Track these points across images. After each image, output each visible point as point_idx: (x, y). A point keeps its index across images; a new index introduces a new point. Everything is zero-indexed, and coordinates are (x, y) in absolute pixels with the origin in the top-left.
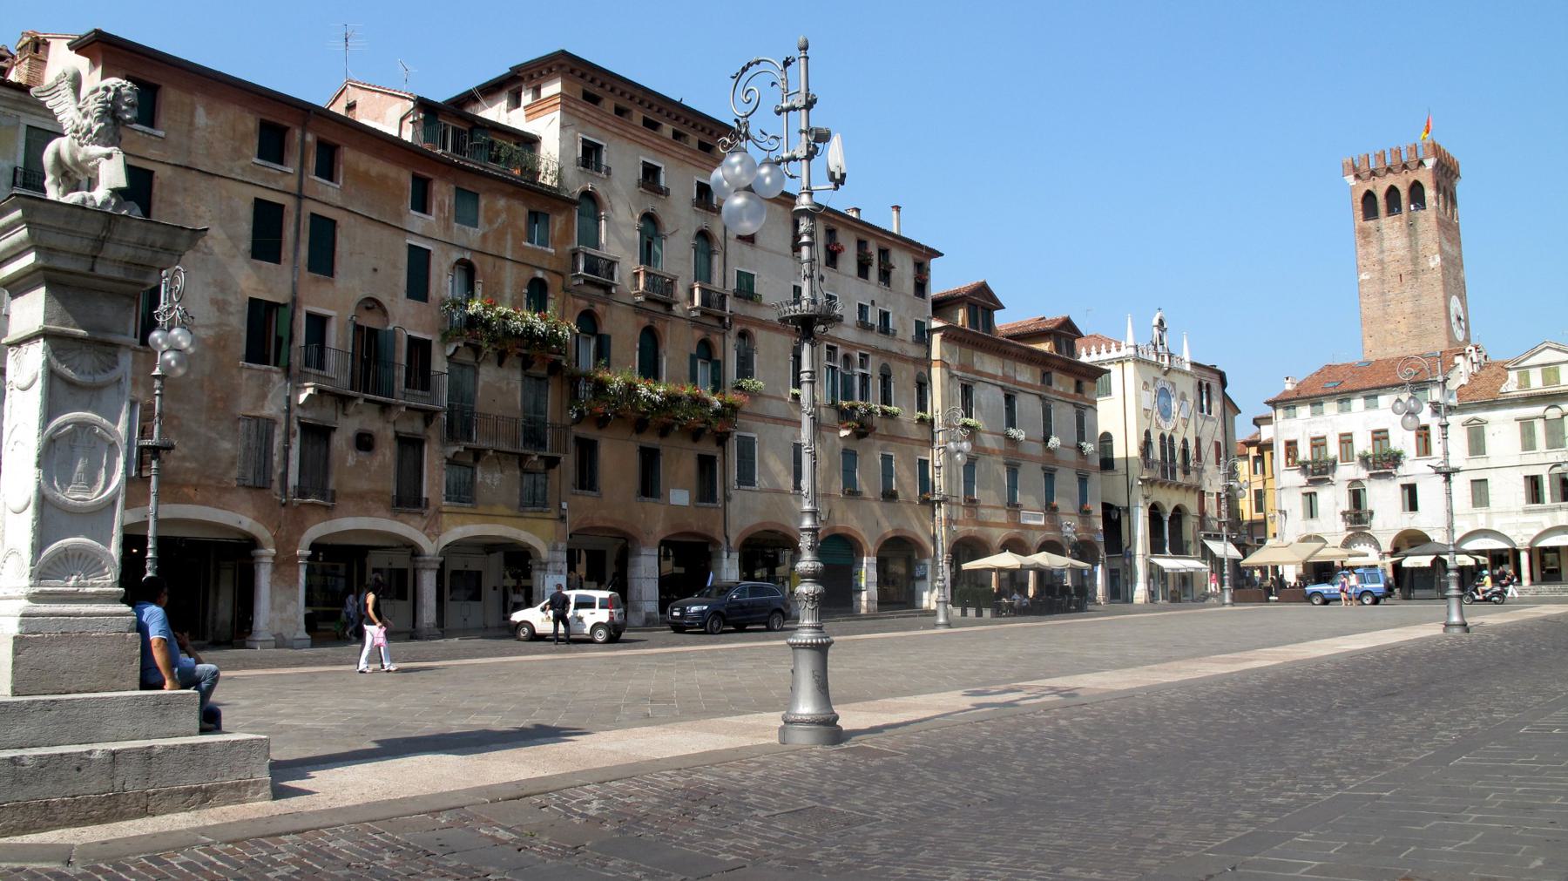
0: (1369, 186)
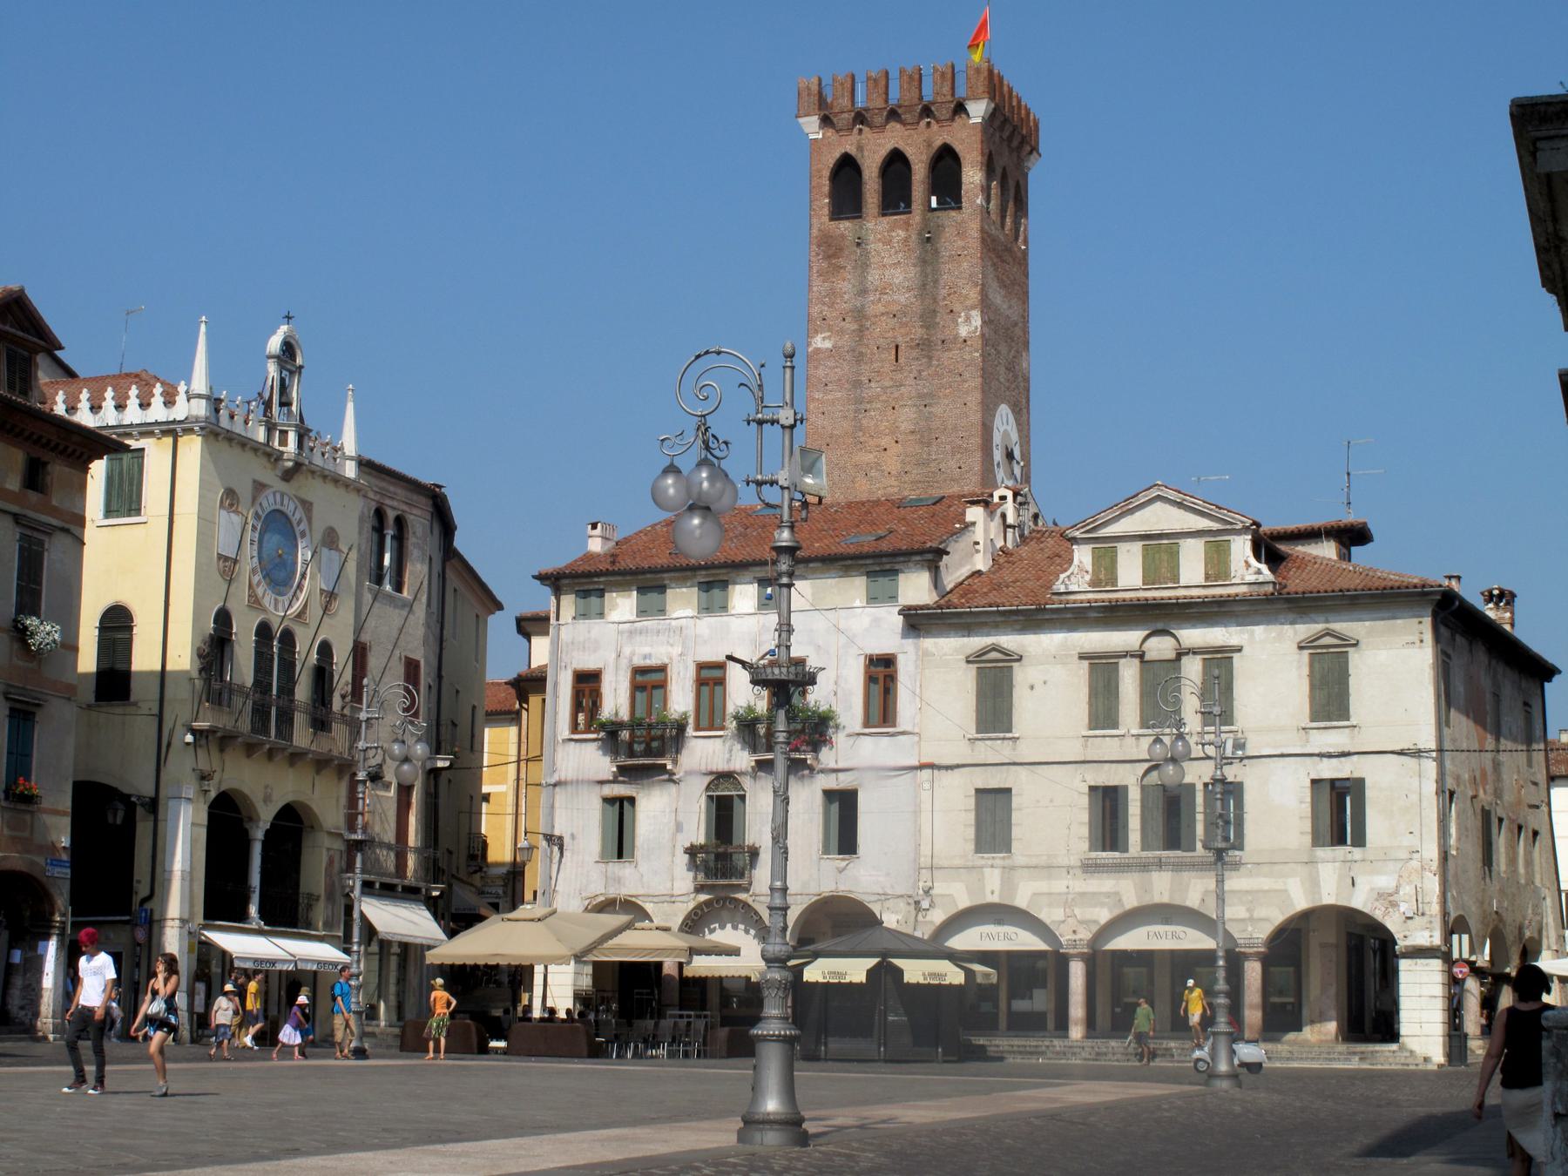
0: (848, 145)
